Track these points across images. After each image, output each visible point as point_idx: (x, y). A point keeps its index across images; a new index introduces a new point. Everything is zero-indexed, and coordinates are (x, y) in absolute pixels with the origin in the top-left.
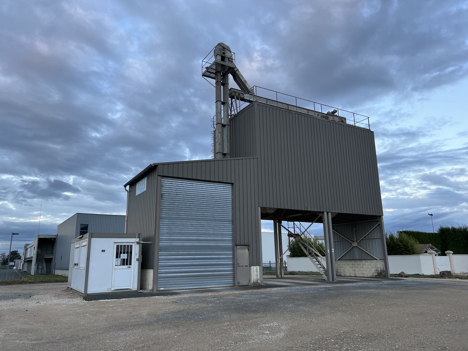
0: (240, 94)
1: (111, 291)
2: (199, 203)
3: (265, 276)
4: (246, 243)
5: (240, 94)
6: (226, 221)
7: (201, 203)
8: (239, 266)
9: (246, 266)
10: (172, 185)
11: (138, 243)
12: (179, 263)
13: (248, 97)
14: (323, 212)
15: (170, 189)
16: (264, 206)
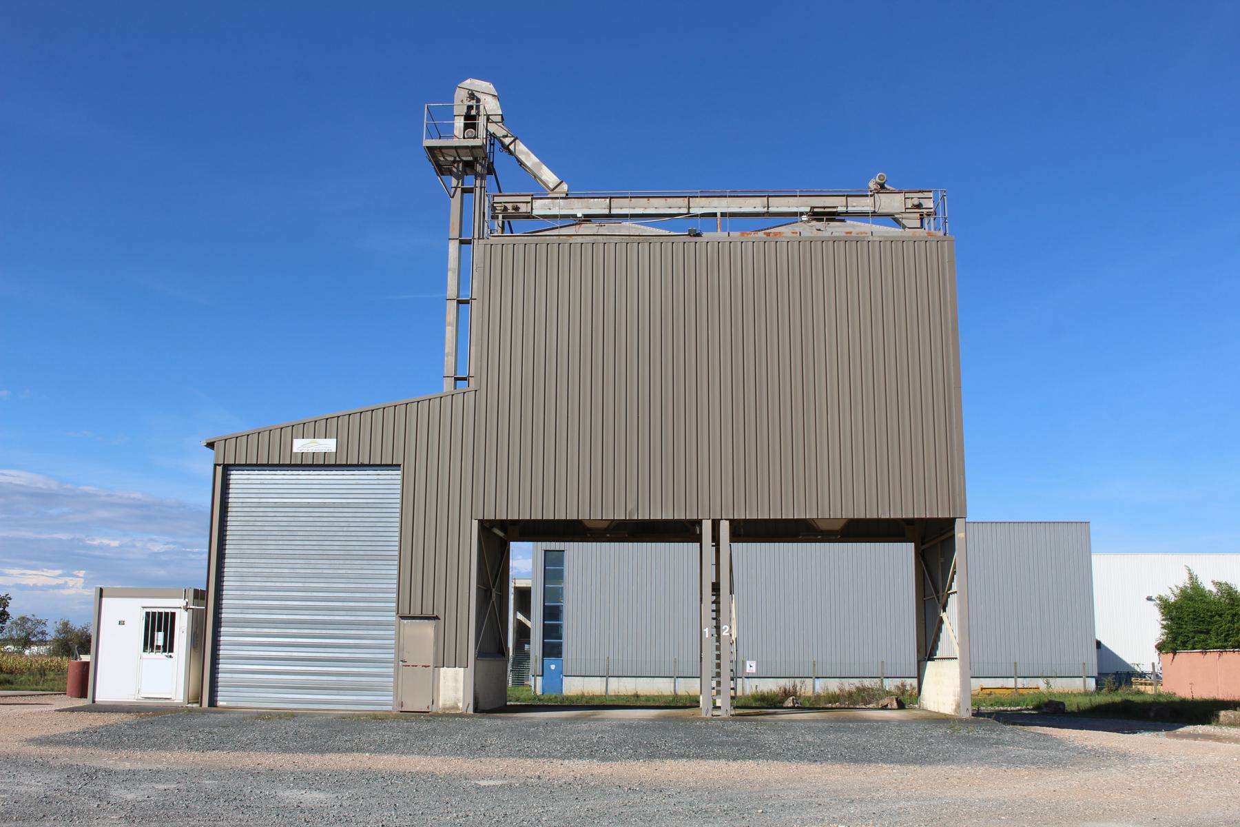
0: (518, 205)
1: (135, 701)
2: (311, 519)
4: (430, 613)
5: (518, 205)
6: (380, 558)
9: (425, 666)
10: (250, 482)
11: (187, 609)
13: (543, 207)
14: (699, 522)
16: (490, 516)
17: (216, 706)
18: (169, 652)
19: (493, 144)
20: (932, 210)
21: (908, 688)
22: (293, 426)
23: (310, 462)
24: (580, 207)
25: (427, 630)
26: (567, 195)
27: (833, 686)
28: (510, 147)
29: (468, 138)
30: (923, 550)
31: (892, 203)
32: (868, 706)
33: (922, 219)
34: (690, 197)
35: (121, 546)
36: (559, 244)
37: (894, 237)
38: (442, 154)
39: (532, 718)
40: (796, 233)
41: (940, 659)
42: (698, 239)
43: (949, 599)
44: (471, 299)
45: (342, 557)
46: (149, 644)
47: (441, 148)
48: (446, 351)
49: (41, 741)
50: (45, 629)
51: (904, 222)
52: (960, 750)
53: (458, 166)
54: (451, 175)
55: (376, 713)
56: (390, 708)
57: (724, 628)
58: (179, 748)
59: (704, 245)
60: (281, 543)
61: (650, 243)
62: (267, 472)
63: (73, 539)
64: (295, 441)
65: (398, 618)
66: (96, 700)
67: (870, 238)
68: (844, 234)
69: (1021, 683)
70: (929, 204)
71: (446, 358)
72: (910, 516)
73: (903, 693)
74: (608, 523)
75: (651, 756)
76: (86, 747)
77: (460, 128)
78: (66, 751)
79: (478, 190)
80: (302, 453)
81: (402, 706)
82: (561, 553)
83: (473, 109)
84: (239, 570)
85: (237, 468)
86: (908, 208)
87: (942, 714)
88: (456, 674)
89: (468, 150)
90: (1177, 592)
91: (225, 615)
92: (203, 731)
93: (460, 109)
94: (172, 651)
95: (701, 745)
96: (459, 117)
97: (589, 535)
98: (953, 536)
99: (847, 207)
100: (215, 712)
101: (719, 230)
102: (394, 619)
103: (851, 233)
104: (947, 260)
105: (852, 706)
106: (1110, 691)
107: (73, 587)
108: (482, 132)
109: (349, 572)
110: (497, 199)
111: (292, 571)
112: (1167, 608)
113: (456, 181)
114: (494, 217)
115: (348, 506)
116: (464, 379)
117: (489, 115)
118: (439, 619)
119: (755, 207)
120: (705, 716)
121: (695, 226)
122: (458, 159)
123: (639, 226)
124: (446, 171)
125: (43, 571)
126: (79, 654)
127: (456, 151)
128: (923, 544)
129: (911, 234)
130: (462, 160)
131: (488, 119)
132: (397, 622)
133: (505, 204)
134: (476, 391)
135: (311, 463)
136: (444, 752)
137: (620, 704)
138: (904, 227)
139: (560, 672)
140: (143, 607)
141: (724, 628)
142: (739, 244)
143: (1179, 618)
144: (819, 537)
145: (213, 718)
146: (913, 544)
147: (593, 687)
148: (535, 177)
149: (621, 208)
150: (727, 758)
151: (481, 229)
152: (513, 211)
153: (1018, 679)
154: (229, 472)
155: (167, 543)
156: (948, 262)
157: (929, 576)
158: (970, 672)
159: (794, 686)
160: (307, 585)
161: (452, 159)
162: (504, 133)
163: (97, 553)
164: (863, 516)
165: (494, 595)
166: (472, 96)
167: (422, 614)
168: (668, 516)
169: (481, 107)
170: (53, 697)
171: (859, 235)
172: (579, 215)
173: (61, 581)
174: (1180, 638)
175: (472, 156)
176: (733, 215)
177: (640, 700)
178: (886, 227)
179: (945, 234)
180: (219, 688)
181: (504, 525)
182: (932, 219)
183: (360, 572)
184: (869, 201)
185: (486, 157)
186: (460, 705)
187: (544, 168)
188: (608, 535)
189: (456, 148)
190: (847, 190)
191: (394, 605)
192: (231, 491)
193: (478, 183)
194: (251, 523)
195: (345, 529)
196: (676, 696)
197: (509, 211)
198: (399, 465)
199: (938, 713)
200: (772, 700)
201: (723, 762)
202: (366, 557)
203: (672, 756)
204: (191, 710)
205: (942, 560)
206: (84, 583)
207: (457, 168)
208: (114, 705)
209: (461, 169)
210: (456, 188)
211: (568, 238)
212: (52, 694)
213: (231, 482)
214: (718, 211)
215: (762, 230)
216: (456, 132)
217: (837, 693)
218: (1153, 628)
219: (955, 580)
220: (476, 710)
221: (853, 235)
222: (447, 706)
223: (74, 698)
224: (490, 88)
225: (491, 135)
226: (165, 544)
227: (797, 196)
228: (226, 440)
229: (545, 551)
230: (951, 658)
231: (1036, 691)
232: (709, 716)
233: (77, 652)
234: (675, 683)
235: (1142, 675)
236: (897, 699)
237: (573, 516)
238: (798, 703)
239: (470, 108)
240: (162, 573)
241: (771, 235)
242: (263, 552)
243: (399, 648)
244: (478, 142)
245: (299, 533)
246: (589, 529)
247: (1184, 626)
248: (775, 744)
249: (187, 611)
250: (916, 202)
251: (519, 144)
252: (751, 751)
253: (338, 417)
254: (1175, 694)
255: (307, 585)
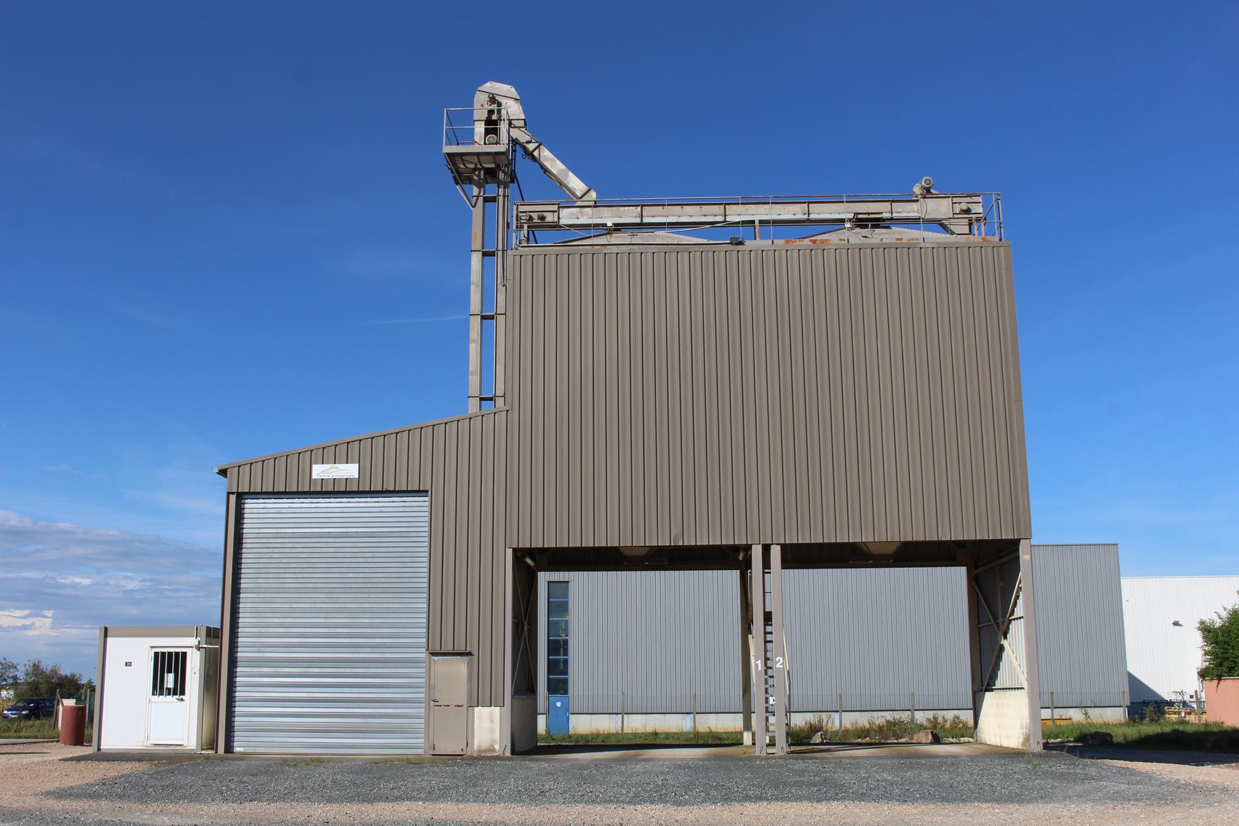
0: (545, 214)
3: (793, 748)
4: (462, 649)
5: (545, 214)
6: (407, 590)
7: (339, 550)
8: (437, 706)
9: (459, 706)
11: (199, 648)
12: (281, 695)
13: (570, 217)
14: (748, 548)
15: (261, 521)
16: (526, 544)
17: (233, 753)
18: (180, 695)
19: (515, 151)
20: (981, 215)
21: (940, 720)
22: (312, 451)
23: (331, 489)
24: (609, 215)
25: (460, 667)
26: (595, 203)
27: (863, 720)
28: (534, 153)
29: (489, 144)
30: (976, 575)
31: (940, 208)
32: (900, 741)
33: (970, 225)
34: (726, 204)
35: (93, 585)
36: (593, 254)
37: (946, 243)
38: (463, 160)
39: (576, 759)
40: (844, 240)
41: (1000, 689)
42: (740, 247)
43: (1010, 626)
44: (496, 314)
45: (367, 590)
46: (158, 687)
47: (462, 155)
48: (471, 369)
49: (48, 794)
50: (16, 673)
51: (952, 228)
52: (1053, 787)
53: (479, 173)
54: (471, 183)
55: (409, 757)
56: (421, 751)
57: (777, 660)
58: (213, 800)
59: (747, 254)
60: (300, 576)
61: (690, 252)
62: (285, 500)
63: (45, 578)
64: (314, 467)
65: (429, 655)
66: (102, 747)
67: (923, 245)
68: (894, 241)
69: (1058, 713)
70: (978, 209)
71: (470, 377)
72: (960, 538)
73: (935, 727)
74: (646, 550)
75: (727, 799)
76: (112, 801)
77: (480, 134)
78: (90, 805)
79: (501, 199)
80: (322, 479)
81: (434, 749)
82: (565, 584)
83: (494, 114)
84: (256, 605)
85: (251, 496)
86: (956, 214)
87: (1006, 747)
88: (492, 714)
89: (491, 157)
90: (1224, 614)
91: (241, 654)
92: (233, 780)
93: (480, 114)
94: (184, 694)
95: (776, 787)
96: (479, 122)
97: (626, 563)
98: (1018, 557)
99: (892, 213)
100: (234, 759)
101: (757, 238)
102: (424, 655)
103: (901, 239)
104: (1004, 267)
105: (883, 741)
106: (1152, 720)
107: (40, 627)
108: (504, 137)
109: (375, 606)
110: (522, 209)
111: (312, 606)
112: (1207, 631)
113: (478, 190)
114: (520, 227)
115: (372, 535)
116: (490, 399)
117: (511, 120)
118: (472, 655)
119: (795, 214)
120: (759, 754)
121: (737, 234)
122: (479, 166)
123: (674, 235)
124: (465, 180)
125: (10, 612)
126: (62, 698)
127: (478, 158)
128: (976, 568)
129: (964, 240)
130: (483, 168)
131: (510, 124)
132: (428, 660)
133: (531, 214)
134: (508, 411)
135: (344, 490)
136: (501, 799)
137: (625, 743)
138: (952, 233)
139: (566, 711)
140: (152, 647)
141: (777, 660)
142: (784, 253)
143: (1225, 643)
144: (871, 562)
145: (230, 766)
146: (738, 571)
147: (605, 724)
148: (561, 184)
149: (654, 217)
150: (810, 798)
151: (507, 240)
152: (539, 221)
153: (843, 713)
154: (243, 501)
155: (143, 581)
156: (1005, 268)
157: (984, 599)
158: (1042, 698)
159: (820, 721)
160: (374, 621)
161: (473, 166)
162: (528, 138)
163: (67, 592)
164: (935, 539)
165: (525, 629)
166: (493, 99)
167: (454, 649)
168: (716, 541)
169: (503, 112)
170: (46, 744)
171: (911, 242)
172: (609, 224)
173: (28, 622)
174: (1226, 664)
175: (495, 163)
176: (775, 222)
177: (659, 738)
178: (930, 233)
179: (1000, 240)
180: (236, 733)
181: (531, 552)
182: (983, 224)
183: (386, 606)
184: (914, 206)
185: (509, 164)
186: (497, 747)
187: (571, 175)
188: (647, 563)
189: (478, 154)
190: (895, 195)
191: (424, 640)
192: (245, 521)
193: (501, 191)
194: (267, 555)
195: (369, 560)
196: (697, 734)
197: (534, 221)
198: (427, 491)
199: (1001, 746)
200: (798, 736)
201: (806, 804)
202: (392, 590)
203: (747, 798)
204: (207, 758)
205: (1001, 584)
206: (52, 623)
207: (479, 176)
208: (122, 753)
209: (482, 177)
210: (478, 197)
211: (602, 248)
212: (44, 742)
213: (246, 511)
214: (757, 218)
215: (808, 237)
216: (477, 138)
217: (1054, 730)
218: (1195, 654)
219: (1018, 605)
220: (513, 752)
221: (904, 241)
222: (483, 748)
223: (69, 746)
224: (512, 92)
225: (513, 140)
226: (140, 582)
227: (843, 202)
228: (239, 466)
229: (549, 582)
230: (1015, 689)
231: (1067, 722)
232: (764, 754)
233: (59, 696)
234: (694, 719)
235: (1171, 704)
236: (932, 733)
237: (614, 543)
238: (826, 739)
239: (491, 112)
240: (135, 611)
241: (818, 242)
242: (281, 586)
243: (430, 687)
244: (501, 148)
245: (320, 565)
246: (625, 556)
247: (1231, 651)
248: (854, 783)
249: (199, 650)
250: (964, 207)
251: (543, 151)
252: (832, 791)
253: (360, 440)
254: (1223, 723)
255: (374, 621)
